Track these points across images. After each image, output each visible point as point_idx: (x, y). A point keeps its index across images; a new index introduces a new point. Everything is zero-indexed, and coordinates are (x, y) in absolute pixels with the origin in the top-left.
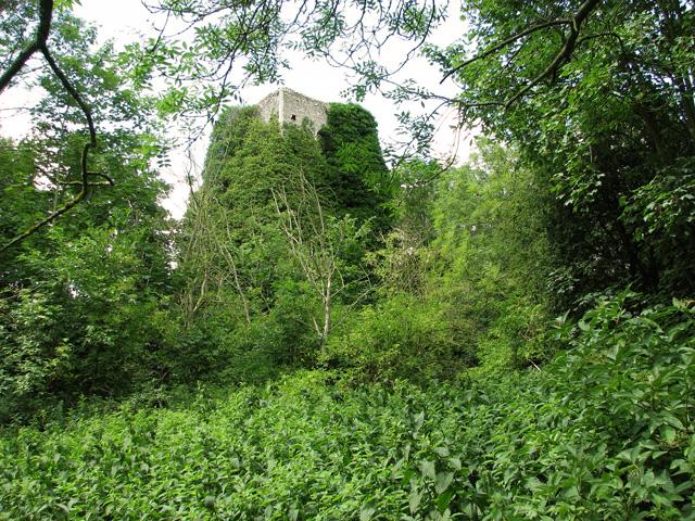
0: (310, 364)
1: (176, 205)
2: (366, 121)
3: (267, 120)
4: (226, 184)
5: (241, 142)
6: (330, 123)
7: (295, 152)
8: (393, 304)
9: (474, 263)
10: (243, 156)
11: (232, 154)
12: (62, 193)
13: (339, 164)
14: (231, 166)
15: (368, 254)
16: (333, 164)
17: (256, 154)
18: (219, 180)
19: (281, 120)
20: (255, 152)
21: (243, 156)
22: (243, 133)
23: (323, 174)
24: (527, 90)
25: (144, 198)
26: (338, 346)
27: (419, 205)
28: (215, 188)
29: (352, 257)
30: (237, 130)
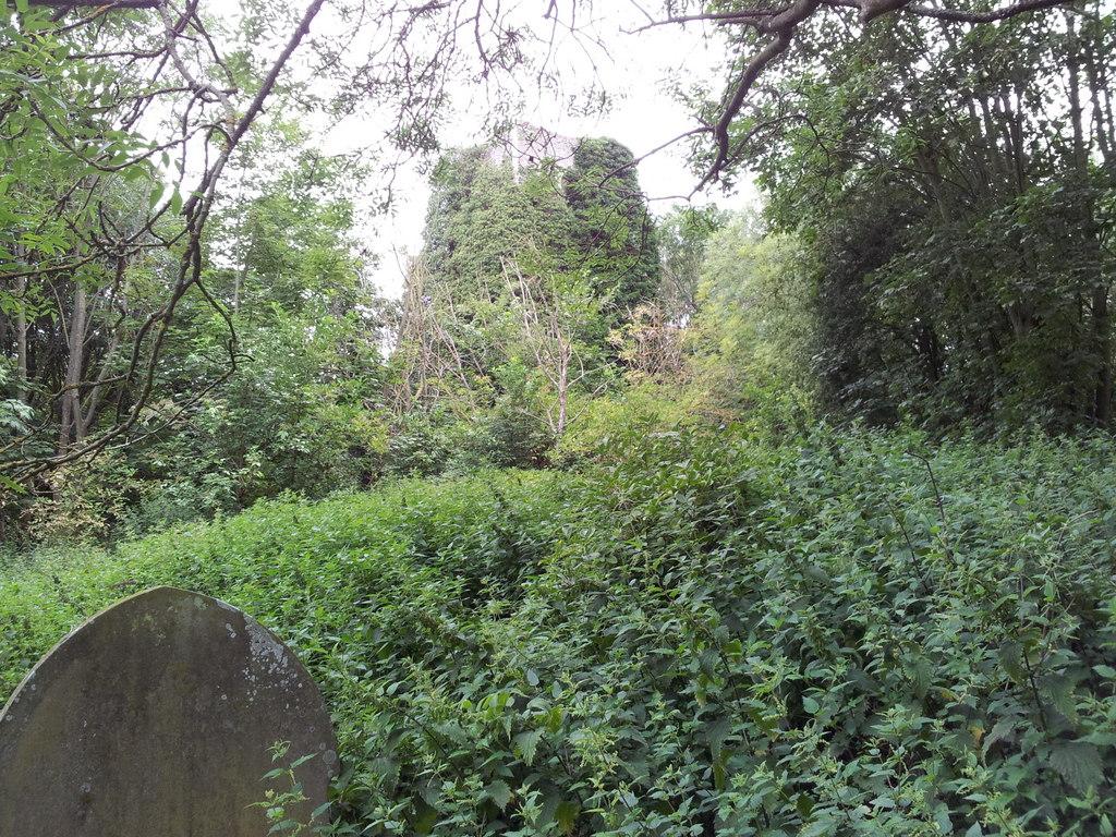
0: (541, 463)
1: (389, 282)
2: (623, 159)
3: (499, 162)
4: (452, 246)
5: (468, 192)
6: (577, 164)
7: (535, 203)
8: (637, 394)
9: (745, 344)
10: (471, 210)
11: (457, 208)
12: (244, 273)
13: (594, 225)
14: (456, 224)
15: (613, 332)
16: (581, 217)
17: (486, 208)
18: (447, 261)
19: (515, 164)
20: (485, 206)
21: (471, 210)
22: (468, 181)
23: (570, 231)
24: (149, 389)
25: (340, 283)
26: (572, 443)
27: (688, 265)
28: (439, 251)
29: (589, 337)
30: (462, 176)
